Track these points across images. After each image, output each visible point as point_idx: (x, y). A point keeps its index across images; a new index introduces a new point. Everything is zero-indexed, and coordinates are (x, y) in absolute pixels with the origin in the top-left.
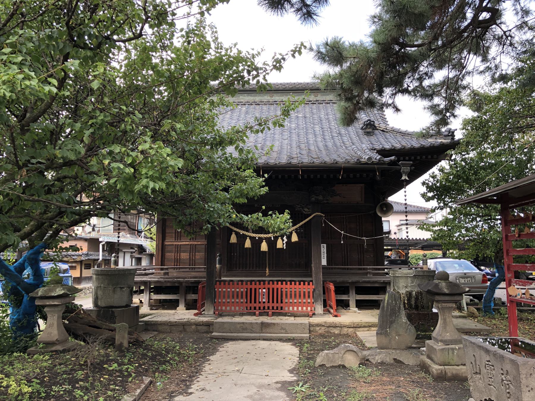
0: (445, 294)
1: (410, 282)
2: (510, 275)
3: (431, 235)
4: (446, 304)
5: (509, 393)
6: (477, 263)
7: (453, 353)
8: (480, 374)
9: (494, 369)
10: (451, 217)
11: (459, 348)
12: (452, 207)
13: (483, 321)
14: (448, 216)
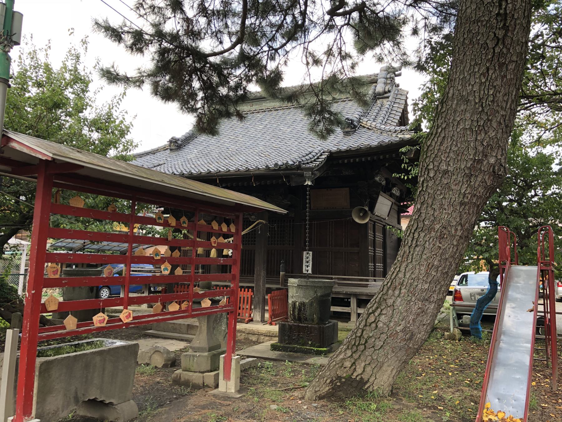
1: (295, 292)
7: (193, 360)
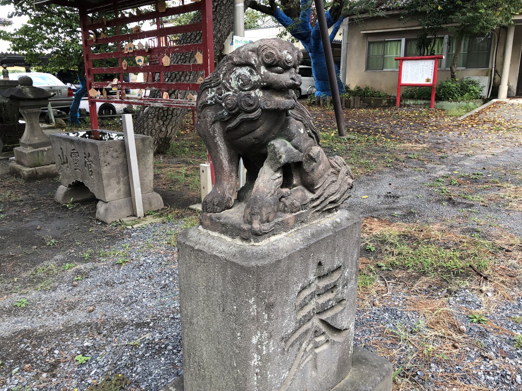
0: (30, 99)
2: (90, 79)
3: (11, 45)
4: (31, 110)
5: (91, 171)
6: (63, 76)
7: (43, 155)
8: (67, 162)
9: (78, 155)
10: (32, 26)
11: (48, 149)
12: (31, 14)
13: (71, 130)
14: (28, 24)
